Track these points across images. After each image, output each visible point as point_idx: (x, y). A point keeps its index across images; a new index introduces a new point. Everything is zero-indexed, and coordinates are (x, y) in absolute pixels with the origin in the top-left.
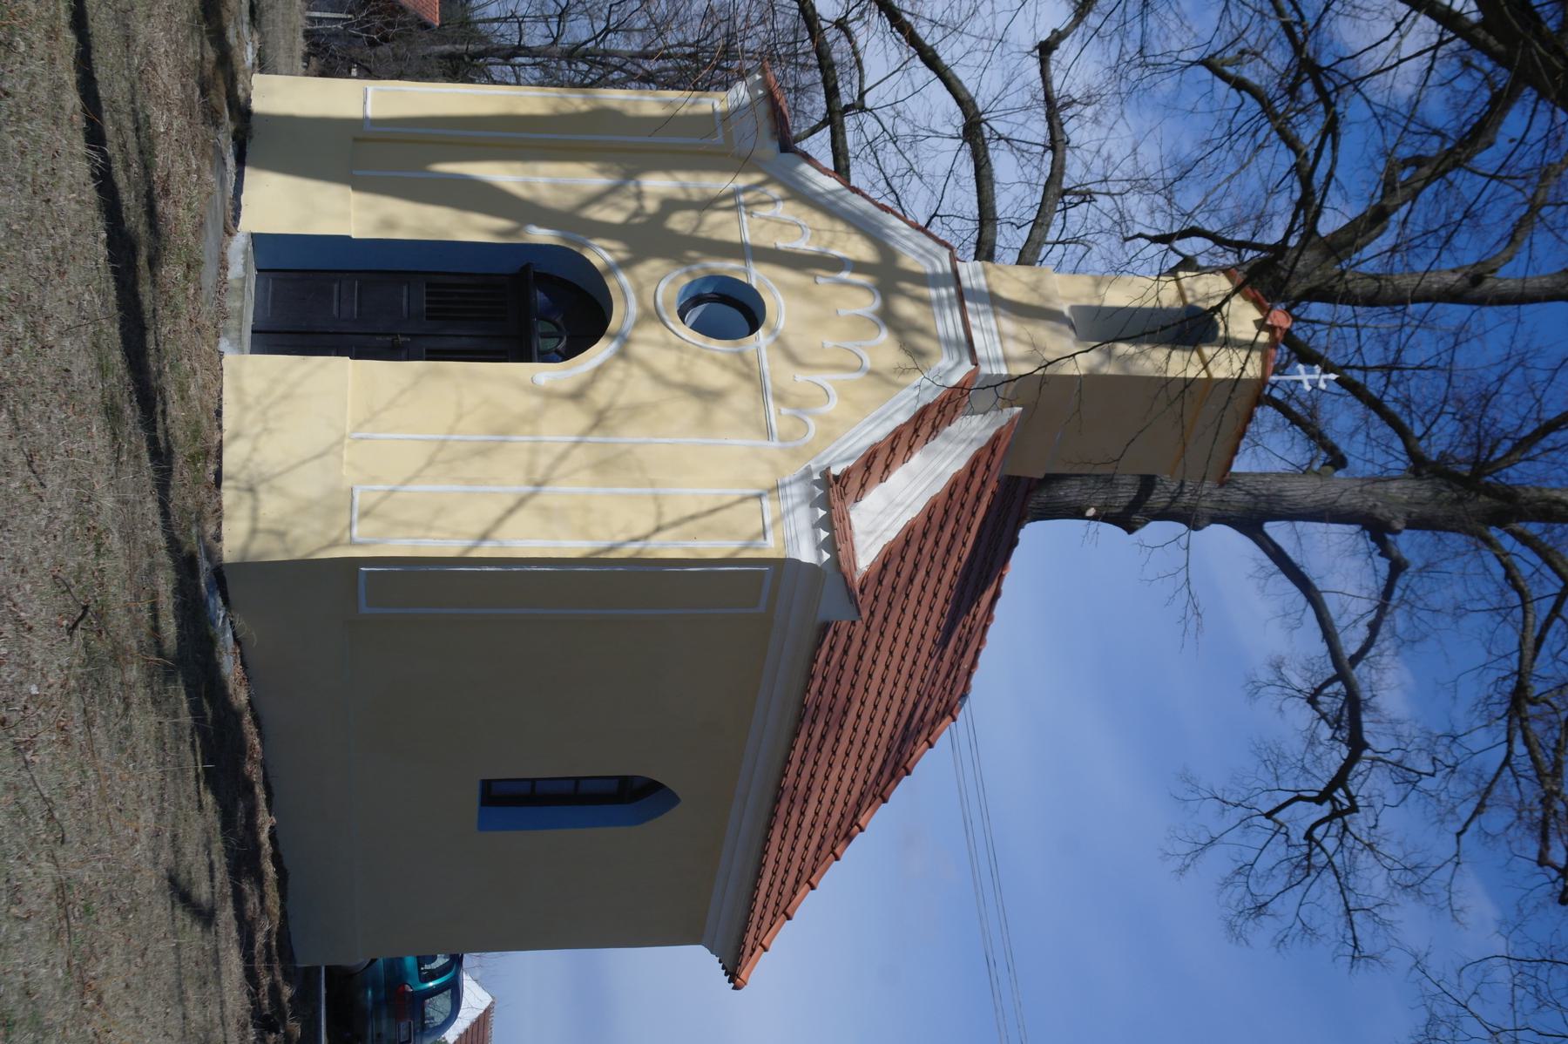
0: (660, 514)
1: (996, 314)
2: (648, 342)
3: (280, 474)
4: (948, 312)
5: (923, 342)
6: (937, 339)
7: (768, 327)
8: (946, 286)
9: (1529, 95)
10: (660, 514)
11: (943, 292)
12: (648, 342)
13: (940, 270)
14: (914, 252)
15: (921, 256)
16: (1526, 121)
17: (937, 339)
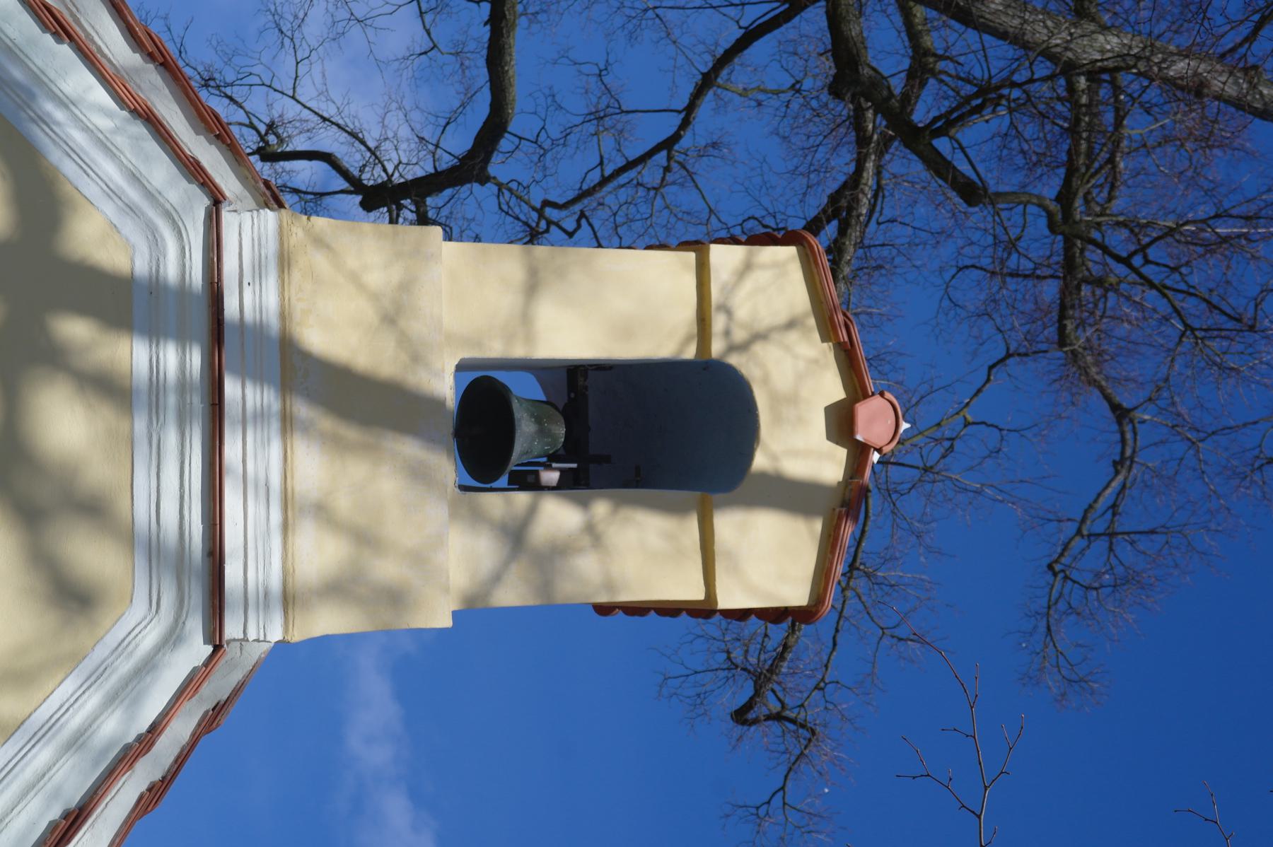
0: (1008, 349)
1: (287, 424)
2: (109, 389)
3: (1135, 408)
4: (171, 438)
5: (92, 555)
6: (127, 536)
7: (750, 255)
8: (182, 339)
9: (432, 171)
10: (1008, 349)
11: (170, 356)
12: (109, 389)
13: (171, 271)
14: (112, 193)
15: (131, 209)
16: (695, 191)
17: (127, 536)
